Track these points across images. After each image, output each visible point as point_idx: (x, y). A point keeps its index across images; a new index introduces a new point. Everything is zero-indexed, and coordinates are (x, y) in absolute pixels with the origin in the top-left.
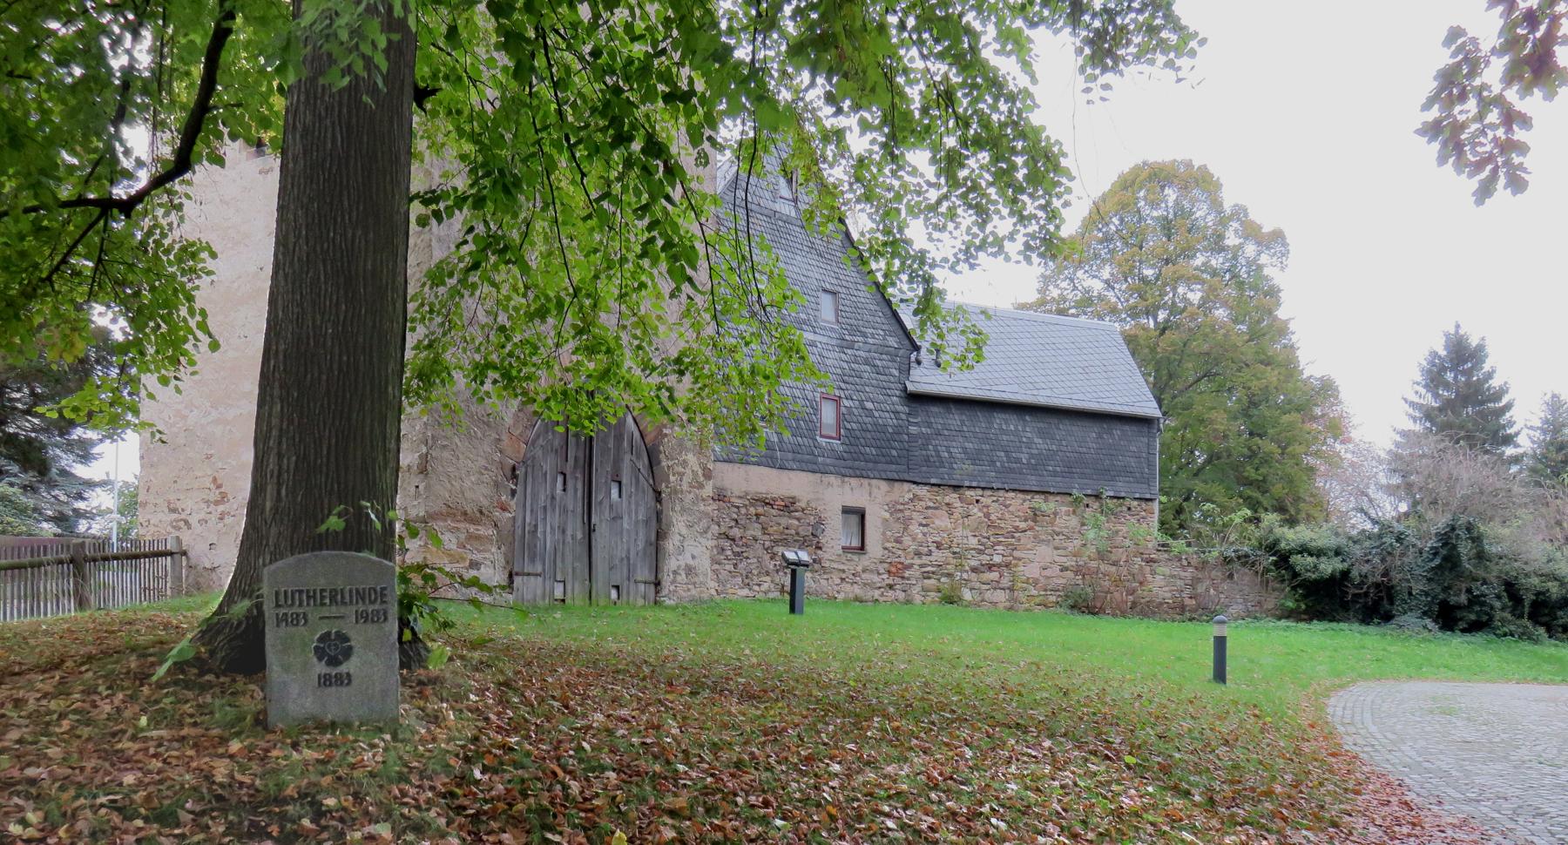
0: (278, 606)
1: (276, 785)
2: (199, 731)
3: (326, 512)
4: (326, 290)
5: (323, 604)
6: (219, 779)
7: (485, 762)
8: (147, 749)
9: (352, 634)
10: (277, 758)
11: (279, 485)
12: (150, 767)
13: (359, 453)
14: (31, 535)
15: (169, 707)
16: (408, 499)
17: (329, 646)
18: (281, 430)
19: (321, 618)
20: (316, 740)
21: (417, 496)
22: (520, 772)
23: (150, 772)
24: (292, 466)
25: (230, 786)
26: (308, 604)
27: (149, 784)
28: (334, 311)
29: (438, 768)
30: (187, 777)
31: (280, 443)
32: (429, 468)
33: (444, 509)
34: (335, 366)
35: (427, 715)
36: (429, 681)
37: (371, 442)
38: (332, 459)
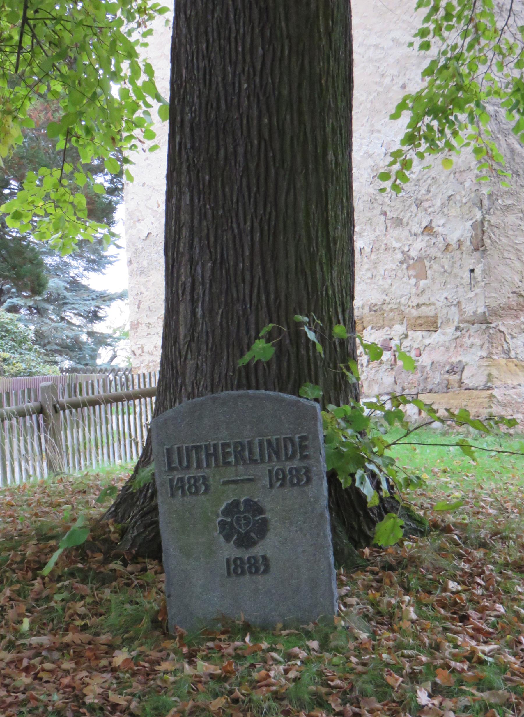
0: (171, 469)
1: (156, 709)
2: (86, 636)
3: (253, 333)
4: (238, 31)
5: (227, 464)
6: (89, 700)
7: (438, 680)
8: (20, 660)
9: (267, 504)
10: (166, 672)
11: (193, 301)
12: (17, 684)
13: (292, 250)
14: (31, 374)
15: (58, 606)
16: (461, 290)
17: (238, 520)
18: (192, 228)
19: (226, 483)
20: (220, 648)
21: (473, 284)
22: (485, 695)
23: (16, 690)
24: (208, 274)
25: (101, 709)
26: (208, 465)
27: (11, 705)
28: (248, 59)
29: (370, 688)
30: (55, 697)
31: (191, 247)
32: (487, 242)
33: (514, 300)
34: (254, 133)
35: (379, 613)
36: (399, 563)
37: (308, 232)
38: (257, 260)
